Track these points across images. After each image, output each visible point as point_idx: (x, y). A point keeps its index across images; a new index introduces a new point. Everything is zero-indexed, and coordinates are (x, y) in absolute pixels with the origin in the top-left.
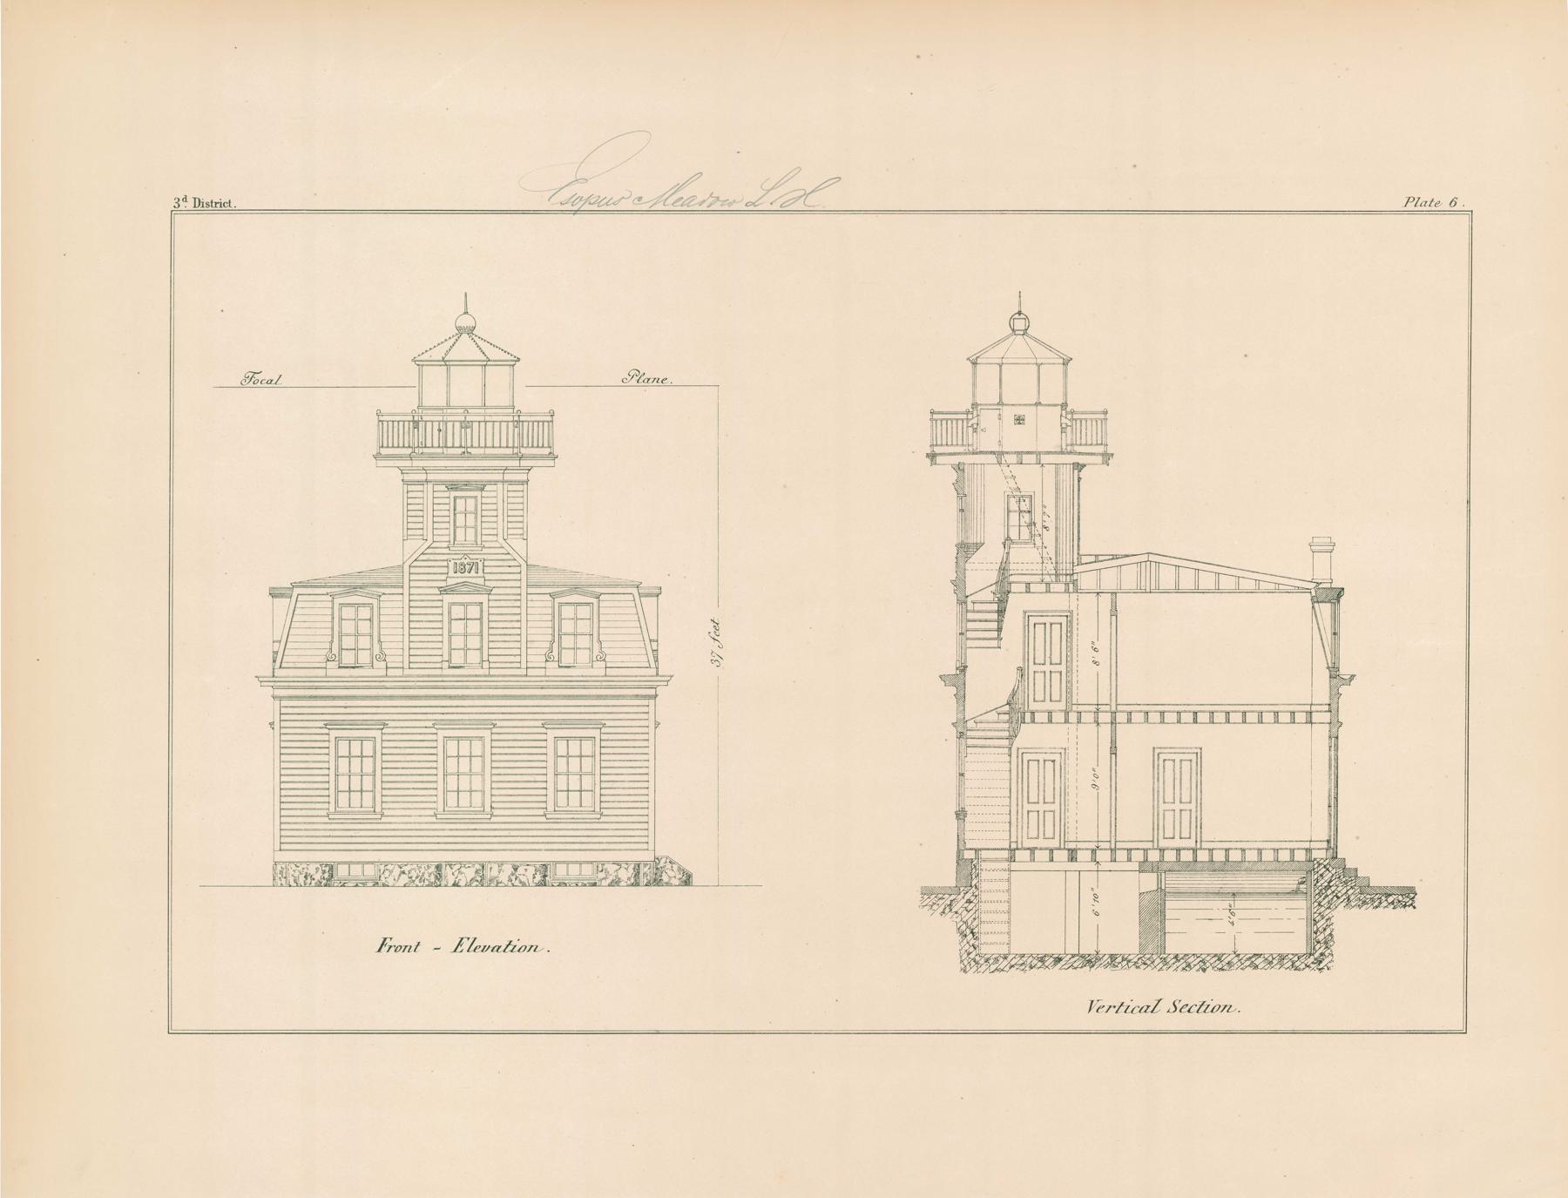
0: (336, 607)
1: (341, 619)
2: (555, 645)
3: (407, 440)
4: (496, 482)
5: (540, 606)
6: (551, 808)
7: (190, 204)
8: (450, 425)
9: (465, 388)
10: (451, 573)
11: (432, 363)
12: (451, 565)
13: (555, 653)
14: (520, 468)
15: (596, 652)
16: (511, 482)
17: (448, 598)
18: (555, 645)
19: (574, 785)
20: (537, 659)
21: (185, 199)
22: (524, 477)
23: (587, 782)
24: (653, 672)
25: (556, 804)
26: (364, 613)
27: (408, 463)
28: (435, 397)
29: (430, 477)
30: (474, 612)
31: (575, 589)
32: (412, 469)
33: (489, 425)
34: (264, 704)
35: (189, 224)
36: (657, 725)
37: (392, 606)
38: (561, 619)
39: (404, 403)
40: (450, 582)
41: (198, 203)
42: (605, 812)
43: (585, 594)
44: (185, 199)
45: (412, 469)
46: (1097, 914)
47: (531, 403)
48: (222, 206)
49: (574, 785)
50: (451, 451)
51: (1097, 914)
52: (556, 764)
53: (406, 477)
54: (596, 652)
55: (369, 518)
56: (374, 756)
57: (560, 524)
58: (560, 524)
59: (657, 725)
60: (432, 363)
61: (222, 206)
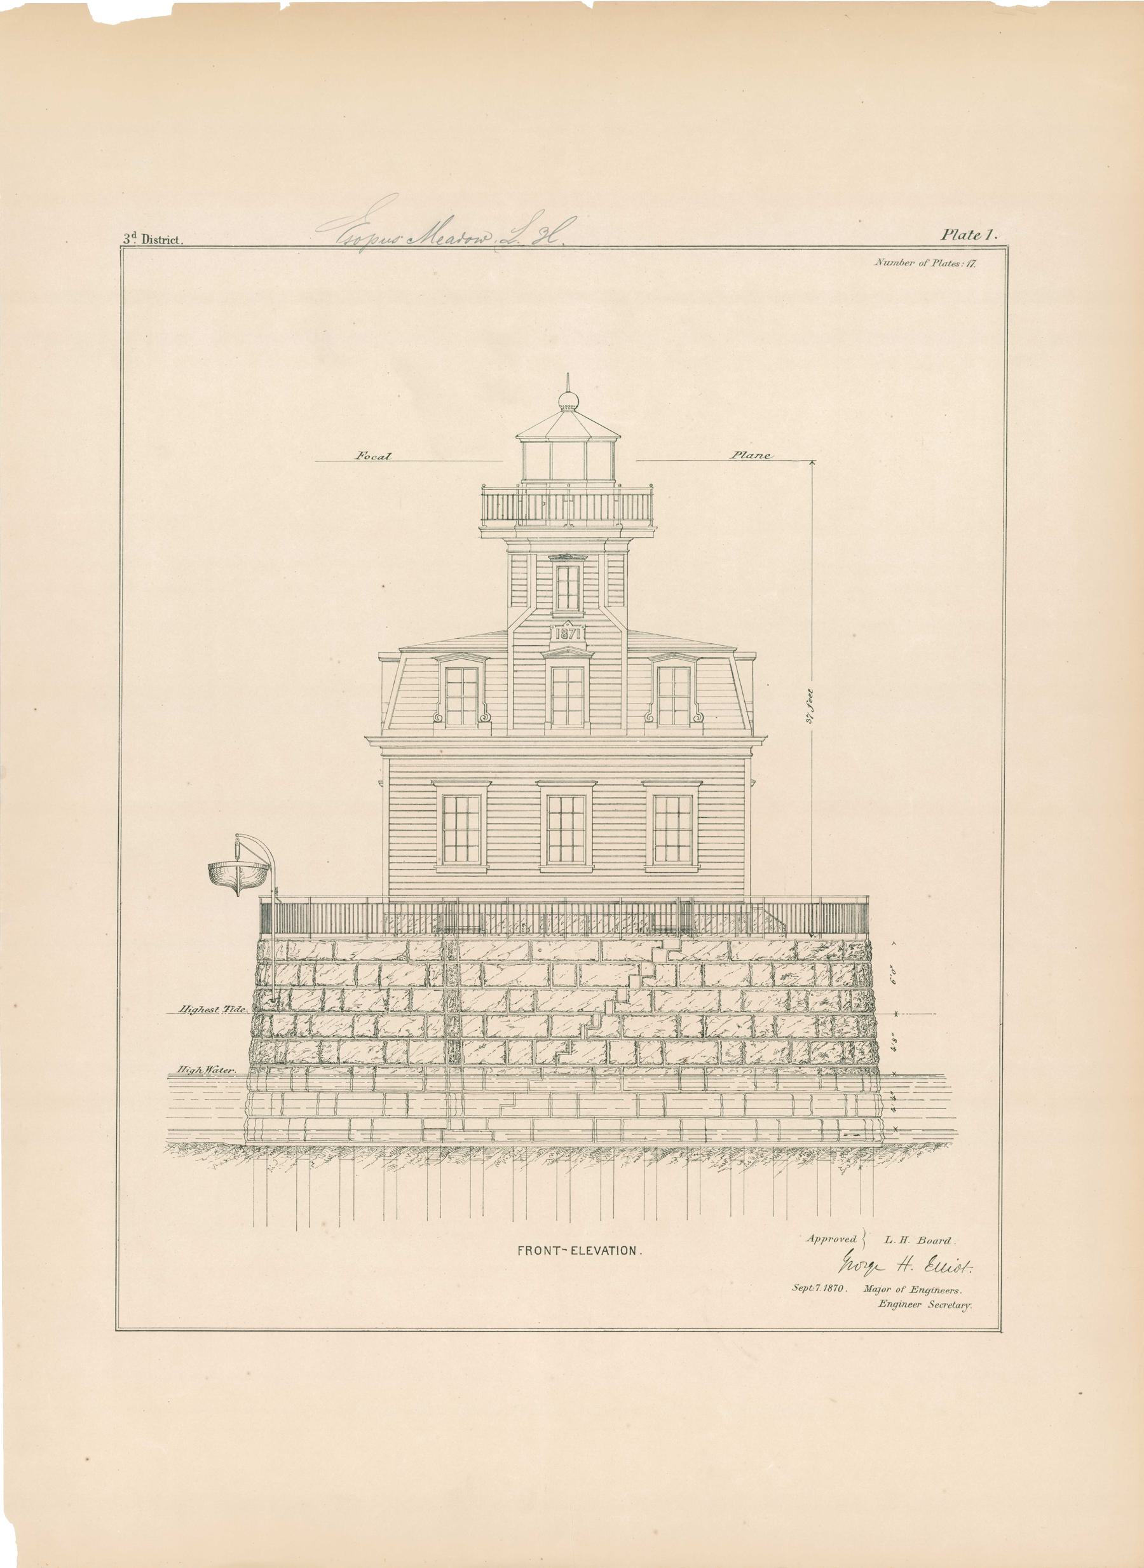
0: (443, 670)
1: (477, 683)
2: (654, 706)
3: (508, 510)
4: (596, 553)
5: (640, 671)
6: (650, 862)
7: (139, 241)
8: (553, 498)
9: (568, 464)
10: (554, 639)
11: (537, 440)
12: (554, 630)
13: (654, 714)
14: (619, 539)
15: (693, 714)
16: (610, 553)
17: (551, 662)
18: (654, 706)
19: (672, 840)
20: (637, 721)
21: (134, 235)
22: (624, 547)
23: (685, 838)
24: (748, 733)
25: (654, 858)
26: (470, 676)
27: (513, 535)
28: (539, 470)
29: (535, 548)
30: (576, 675)
31: (674, 654)
32: (517, 539)
33: (591, 498)
34: (373, 764)
35: (137, 257)
36: (753, 783)
37: (496, 669)
38: (659, 683)
39: (507, 477)
40: (553, 646)
41: (147, 239)
42: (492, 866)
43: (685, 657)
44: (134, 235)
45: (517, 539)
46: (893, 982)
47: (631, 476)
48: (171, 243)
49: (672, 840)
50: (553, 523)
51: (893, 982)
52: (548, 821)
53: (512, 548)
54: (693, 714)
55: (474, 590)
56: (480, 813)
57: (664, 592)
58: (664, 592)
59: (753, 783)
60: (537, 440)
61: (171, 243)
